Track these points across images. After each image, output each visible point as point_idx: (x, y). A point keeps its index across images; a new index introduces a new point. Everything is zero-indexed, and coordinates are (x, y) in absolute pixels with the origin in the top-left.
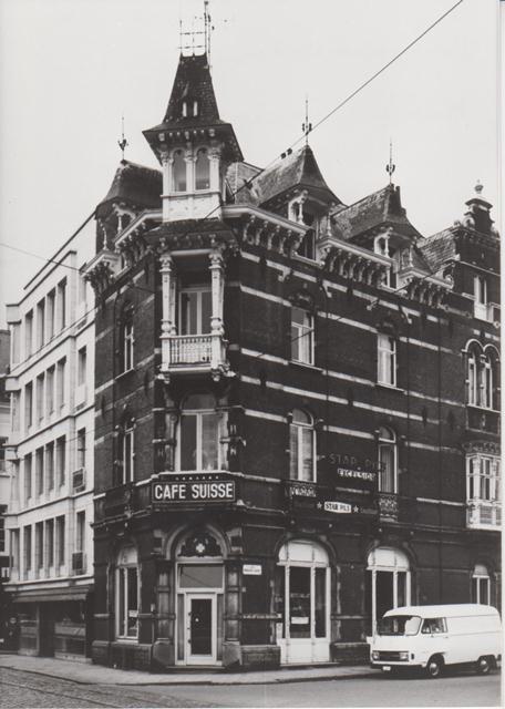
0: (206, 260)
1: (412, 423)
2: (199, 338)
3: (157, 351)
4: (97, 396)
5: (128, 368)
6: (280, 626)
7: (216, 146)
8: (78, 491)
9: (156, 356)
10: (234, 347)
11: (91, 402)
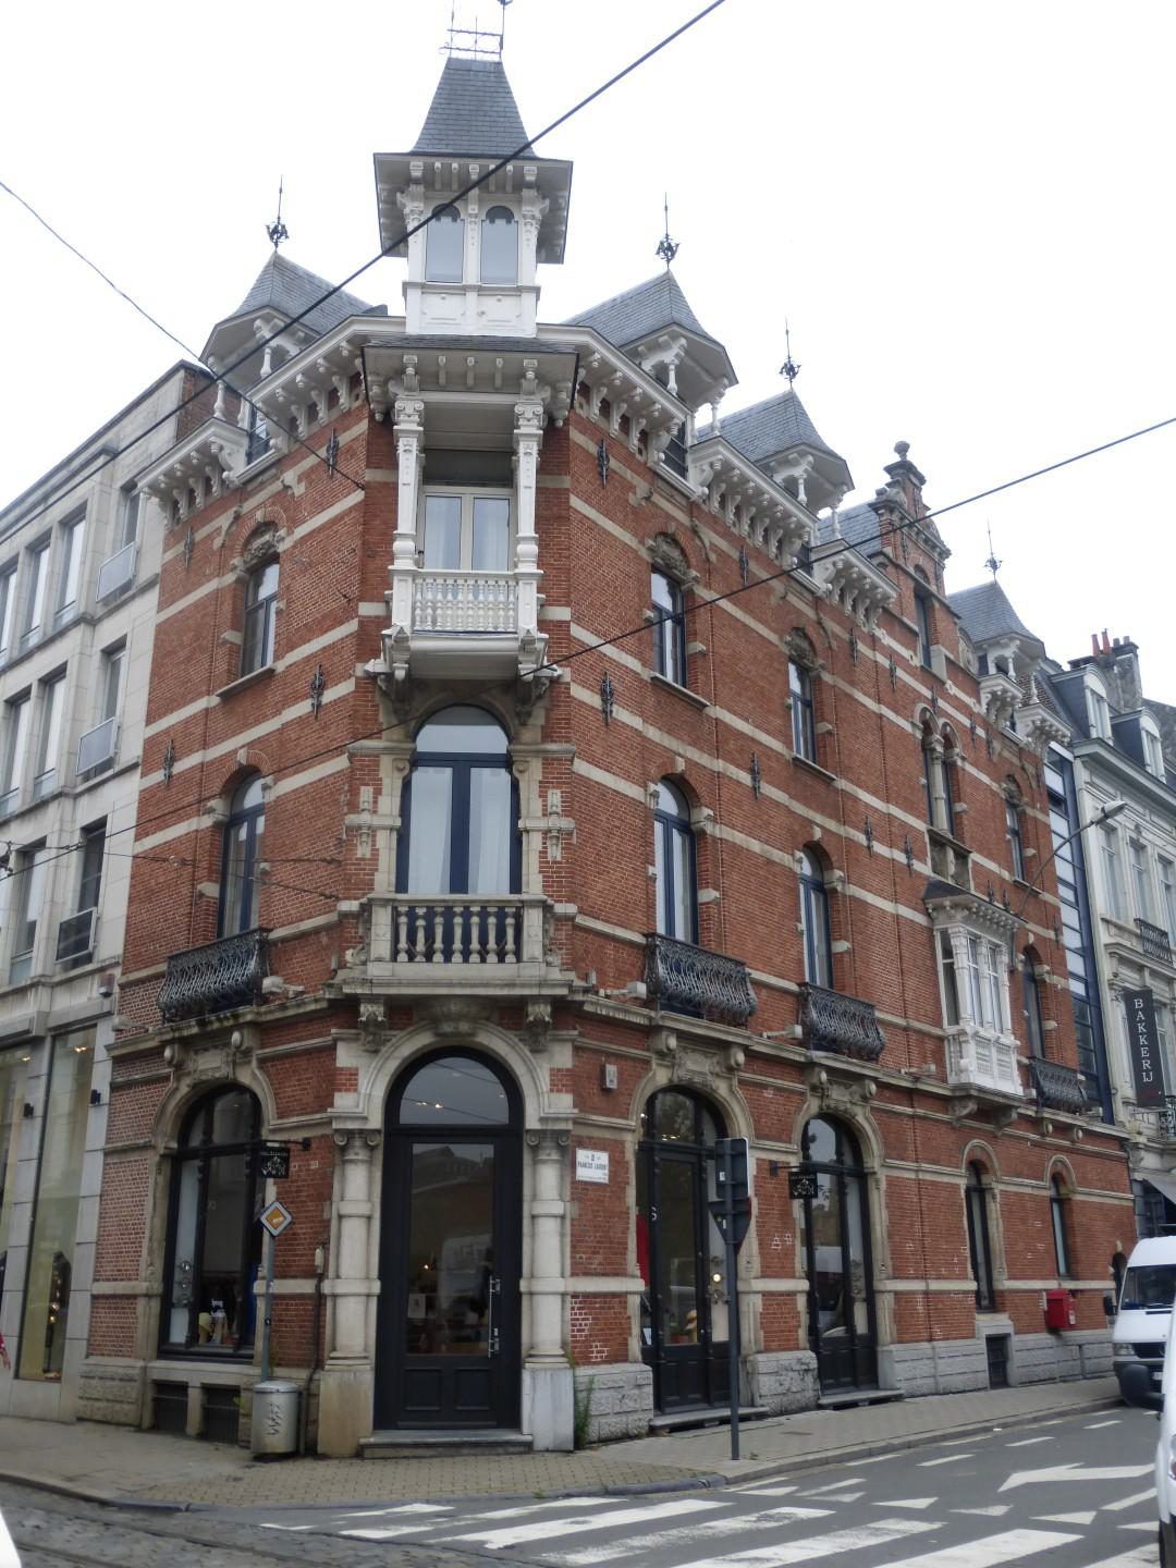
0: (509, 420)
1: (889, 889)
2: (466, 577)
3: (367, 609)
4: (150, 744)
5: (263, 665)
6: (1088, 1351)
7: (532, 203)
8: (66, 969)
9: (365, 623)
10: (562, 613)
11: (132, 751)
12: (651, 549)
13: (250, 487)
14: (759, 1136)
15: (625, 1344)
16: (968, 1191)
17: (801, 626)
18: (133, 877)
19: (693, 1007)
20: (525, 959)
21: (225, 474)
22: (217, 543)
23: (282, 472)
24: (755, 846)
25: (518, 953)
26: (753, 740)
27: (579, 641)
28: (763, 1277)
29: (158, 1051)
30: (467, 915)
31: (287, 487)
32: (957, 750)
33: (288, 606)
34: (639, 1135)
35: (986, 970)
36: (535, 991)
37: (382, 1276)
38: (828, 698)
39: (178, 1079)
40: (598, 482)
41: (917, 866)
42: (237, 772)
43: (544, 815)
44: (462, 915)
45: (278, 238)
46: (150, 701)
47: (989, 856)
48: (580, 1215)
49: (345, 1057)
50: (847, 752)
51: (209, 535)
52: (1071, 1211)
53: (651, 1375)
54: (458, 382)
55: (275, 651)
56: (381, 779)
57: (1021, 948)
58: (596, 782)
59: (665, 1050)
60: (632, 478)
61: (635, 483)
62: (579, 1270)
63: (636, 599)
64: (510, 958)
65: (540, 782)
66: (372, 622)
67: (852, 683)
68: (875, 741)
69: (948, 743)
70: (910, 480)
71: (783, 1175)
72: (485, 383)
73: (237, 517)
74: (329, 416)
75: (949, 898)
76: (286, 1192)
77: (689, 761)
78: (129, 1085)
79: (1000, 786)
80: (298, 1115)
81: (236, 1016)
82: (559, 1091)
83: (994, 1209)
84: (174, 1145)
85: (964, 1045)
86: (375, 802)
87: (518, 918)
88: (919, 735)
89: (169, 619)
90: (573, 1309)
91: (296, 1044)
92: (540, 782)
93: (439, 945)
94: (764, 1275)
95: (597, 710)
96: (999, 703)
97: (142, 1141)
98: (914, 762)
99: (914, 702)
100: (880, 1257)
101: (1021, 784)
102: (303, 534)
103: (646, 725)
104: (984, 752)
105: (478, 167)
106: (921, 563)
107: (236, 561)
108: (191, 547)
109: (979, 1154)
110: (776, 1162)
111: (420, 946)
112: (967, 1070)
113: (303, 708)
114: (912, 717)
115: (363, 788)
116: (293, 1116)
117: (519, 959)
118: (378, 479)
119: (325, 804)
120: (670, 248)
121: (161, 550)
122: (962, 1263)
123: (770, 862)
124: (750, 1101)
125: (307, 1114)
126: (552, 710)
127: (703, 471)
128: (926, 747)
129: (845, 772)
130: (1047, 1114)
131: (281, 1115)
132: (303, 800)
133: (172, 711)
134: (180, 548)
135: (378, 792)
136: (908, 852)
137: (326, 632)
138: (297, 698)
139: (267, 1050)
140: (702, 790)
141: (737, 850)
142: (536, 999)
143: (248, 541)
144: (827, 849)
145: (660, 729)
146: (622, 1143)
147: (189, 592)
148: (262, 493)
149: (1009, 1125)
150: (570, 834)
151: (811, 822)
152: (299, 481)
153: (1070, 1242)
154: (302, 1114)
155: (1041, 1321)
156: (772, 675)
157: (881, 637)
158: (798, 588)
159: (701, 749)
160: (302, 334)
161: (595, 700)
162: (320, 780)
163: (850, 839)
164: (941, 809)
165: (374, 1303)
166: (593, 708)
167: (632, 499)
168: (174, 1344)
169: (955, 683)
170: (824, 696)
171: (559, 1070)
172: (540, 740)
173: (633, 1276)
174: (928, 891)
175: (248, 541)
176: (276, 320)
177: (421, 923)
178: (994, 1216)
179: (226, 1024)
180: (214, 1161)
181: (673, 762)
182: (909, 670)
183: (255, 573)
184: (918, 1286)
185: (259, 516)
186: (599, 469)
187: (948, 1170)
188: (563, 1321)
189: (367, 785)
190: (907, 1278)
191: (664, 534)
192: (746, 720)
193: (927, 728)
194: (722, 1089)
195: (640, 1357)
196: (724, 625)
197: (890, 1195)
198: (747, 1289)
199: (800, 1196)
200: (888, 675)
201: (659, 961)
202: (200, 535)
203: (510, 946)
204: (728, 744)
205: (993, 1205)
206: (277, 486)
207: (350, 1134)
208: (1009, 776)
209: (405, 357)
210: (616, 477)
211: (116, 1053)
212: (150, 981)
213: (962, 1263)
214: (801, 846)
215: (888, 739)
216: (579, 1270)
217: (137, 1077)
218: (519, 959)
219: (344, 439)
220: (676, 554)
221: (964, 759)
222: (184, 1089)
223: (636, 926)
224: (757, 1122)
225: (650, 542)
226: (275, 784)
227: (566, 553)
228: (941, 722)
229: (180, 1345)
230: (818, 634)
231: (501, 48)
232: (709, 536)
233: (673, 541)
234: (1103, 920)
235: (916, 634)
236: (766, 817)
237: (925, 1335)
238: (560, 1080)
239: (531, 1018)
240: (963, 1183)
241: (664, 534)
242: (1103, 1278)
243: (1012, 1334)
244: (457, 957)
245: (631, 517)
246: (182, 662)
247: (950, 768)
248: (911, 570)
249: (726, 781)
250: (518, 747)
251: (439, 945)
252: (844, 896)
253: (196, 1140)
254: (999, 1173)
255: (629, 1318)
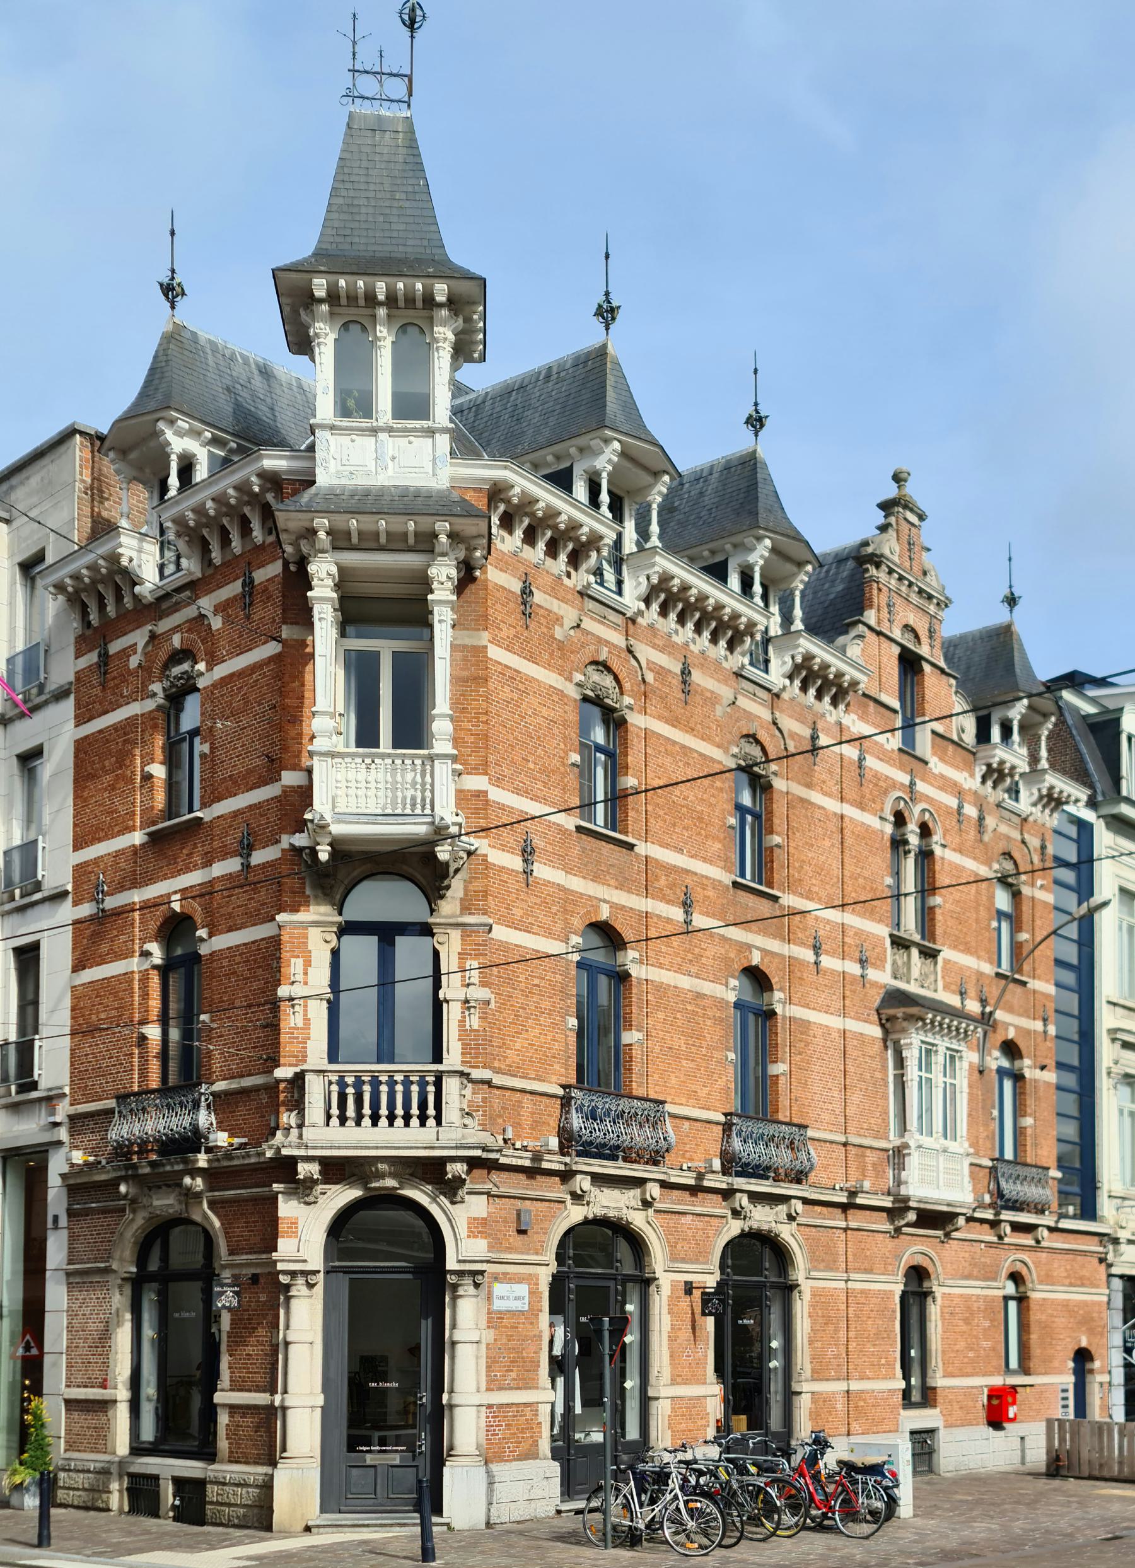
4: (80, 871)
12: (579, 685)
13: (164, 606)
14: (674, 1259)
15: (535, 1444)
16: (904, 1296)
17: (751, 732)
18: (73, 1009)
19: (609, 1152)
20: (444, 1124)
21: (137, 589)
22: (134, 662)
23: (198, 597)
24: (685, 982)
25: (438, 1119)
26: (687, 872)
27: (498, 804)
28: (672, 1384)
29: (114, 1183)
30: (392, 1083)
31: (202, 617)
32: (935, 838)
33: (212, 752)
34: (553, 1267)
35: (938, 1077)
36: (452, 1153)
37: (325, 1390)
38: (780, 808)
39: (134, 1211)
40: (521, 623)
41: (872, 974)
42: (170, 917)
43: (462, 986)
44: (387, 1083)
45: (174, 297)
46: (75, 825)
47: (967, 950)
48: (495, 1340)
49: (287, 1208)
50: (797, 865)
51: (124, 650)
52: (1028, 1309)
53: (558, 1469)
54: (369, 542)
55: (202, 797)
56: (310, 952)
57: (998, 1044)
58: (516, 945)
59: (579, 1192)
60: (559, 607)
61: (561, 613)
62: (493, 1385)
63: (562, 746)
64: (431, 1122)
65: (459, 954)
66: (295, 792)
67: (809, 786)
68: (833, 845)
69: (925, 831)
70: (905, 519)
71: (697, 1294)
72: (396, 543)
73: (153, 637)
74: (243, 546)
75: (903, 1010)
76: (240, 1319)
77: (614, 906)
78: (87, 1212)
79: (991, 868)
80: (247, 1254)
81: (186, 1161)
82: (475, 1237)
83: (934, 1311)
84: (134, 1270)
85: (906, 1159)
86: (306, 974)
87: (438, 1084)
88: (889, 829)
89: (87, 737)
90: (488, 1417)
91: (242, 1191)
92: (459, 954)
93: (367, 1111)
94: (674, 1382)
95: (517, 872)
96: (996, 775)
97: (102, 1265)
98: (879, 862)
99: (886, 792)
100: (799, 1361)
101: (1019, 861)
102: (223, 674)
103: (569, 876)
104: (972, 833)
105: (384, 284)
106: (911, 623)
107: (156, 687)
108: (105, 657)
109: (920, 1260)
110: (691, 1283)
111: (351, 1112)
112: (906, 1183)
113: (232, 865)
114: (882, 810)
115: (293, 960)
116: (242, 1254)
117: (439, 1123)
118: (295, 637)
119: (258, 967)
120: (612, 310)
121: (73, 657)
122: (891, 1366)
123: (699, 996)
124: (667, 1230)
125: (255, 1253)
126: (471, 882)
127: (639, 584)
128: (898, 844)
129: (790, 888)
130: (1006, 1215)
131: (231, 1253)
132: (237, 959)
133: (100, 840)
134: (92, 657)
135: (308, 964)
136: (863, 962)
137: (251, 789)
138: (225, 855)
139: (217, 1193)
140: (628, 935)
141: (661, 989)
142: (454, 1159)
143: (166, 666)
144: (767, 972)
145: (584, 878)
146: (537, 1276)
147: (106, 712)
148: (177, 615)
149: (957, 1230)
150: (488, 1002)
151: (749, 947)
152: (216, 611)
153: (1025, 1338)
154: (250, 1253)
155: (982, 1414)
156: (713, 796)
157: (850, 725)
158: (751, 687)
159: (629, 891)
160: (208, 435)
161: (515, 863)
162: (253, 942)
163: (794, 958)
164: (910, 906)
165: (319, 1411)
166: (513, 870)
167: (559, 633)
168: (144, 1442)
169: (942, 759)
170: (775, 806)
171: (475, 1219)
172: (458, 912)
173: (545, 1389)
174: (883, 1001)
175: (166, 666)
176: (179, 422)
177: (350, 1090)
178: (933, 1318)
179: (176, 1168)
180: (171, 1285)
181: (597, 909)
182: (884, 755)
183: (176, 699)
184: (841, 1386)
185: (176, 641)
186: (522, 607)
187: (882, 1278)
188: (478, 1428)
189: (298, 957)
190: (827, 1380)
191: (595, 663)
192: (681, 851)
193: (900, 819)
194: (638, 1220)
195: (550, 1455)
196: (660, 752)
197: (813, 1305)
198: (656, 1395)
199: (710, 1314)
200: (855, 767)
201: (574, 1111)
202: (114, 647)
203: (431, 1111)
204: (658, 881)
205: (933, 1306)
206: (190, 612)
207: (293, 1274)
208: (1004, 854)
209: (316, 521)
210: (542, 612)
211: (71, 1182)
212: (99, 1115)
213: (891, 1366)
214: (737, 974)
215: (849, 841)
216: (493, 1385)
217: (94, 1205)
218: (439, 1123)
219: (261, 575)
220: (608, 681)
221: (944, 846)
222: (140, 1221)
223: (554, 1078)
224: (673, 1246)
225: (578, 677)
226: (210, 937)
227: (483, 718)
228: (917, 810)
229: (150, 1443)
230: (773, 736)
231: (410, 95)
232: (645, 653)
233: (604, 666)
234: (1109, 1002)
235: (895, 711)
236: (697, 950)
237: (844, 1430)
238: (479, 1227)
239: (450, 1176)
240: (898, 1289)
241: (595, 663)
242: (1060, 1372)
243: (941, 1427)
244: (383, 1122)
245: (557, 653)
246: (106, 789)
247: (926, 856)
248: (897, 634)
249: (655, 920)
250: (438, 920)
251: (367, 1111)
252: (784, 1017)
253: (153, 1266)
254: (941, 1277)
255: (540, 1423)
